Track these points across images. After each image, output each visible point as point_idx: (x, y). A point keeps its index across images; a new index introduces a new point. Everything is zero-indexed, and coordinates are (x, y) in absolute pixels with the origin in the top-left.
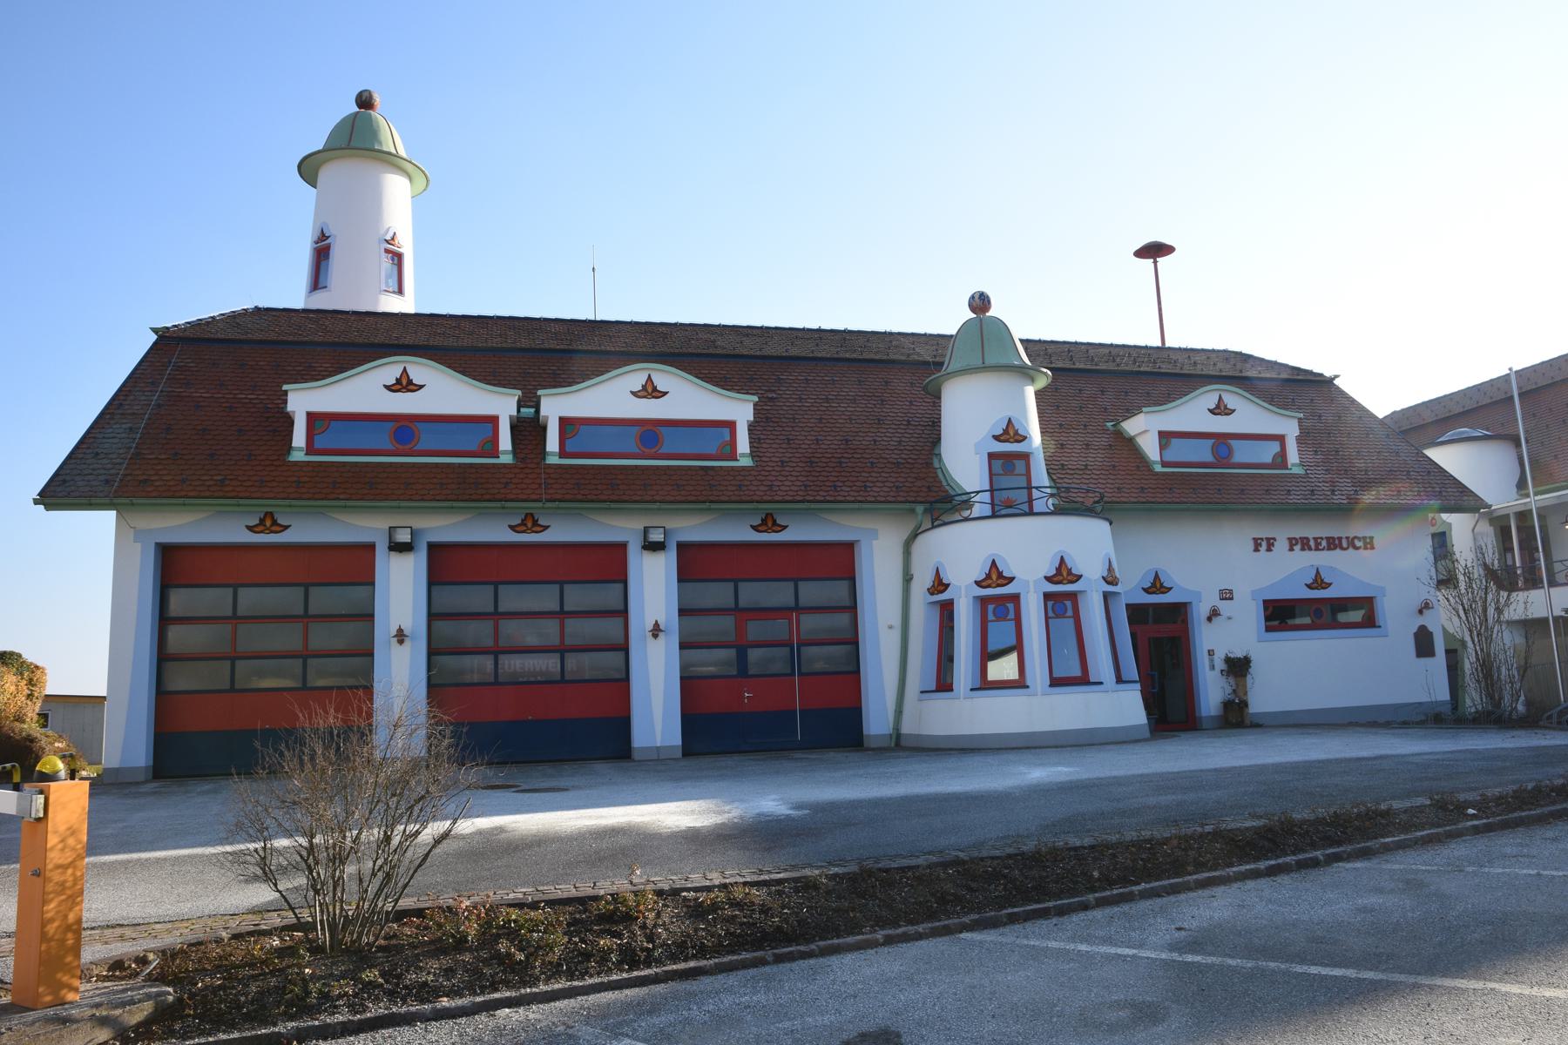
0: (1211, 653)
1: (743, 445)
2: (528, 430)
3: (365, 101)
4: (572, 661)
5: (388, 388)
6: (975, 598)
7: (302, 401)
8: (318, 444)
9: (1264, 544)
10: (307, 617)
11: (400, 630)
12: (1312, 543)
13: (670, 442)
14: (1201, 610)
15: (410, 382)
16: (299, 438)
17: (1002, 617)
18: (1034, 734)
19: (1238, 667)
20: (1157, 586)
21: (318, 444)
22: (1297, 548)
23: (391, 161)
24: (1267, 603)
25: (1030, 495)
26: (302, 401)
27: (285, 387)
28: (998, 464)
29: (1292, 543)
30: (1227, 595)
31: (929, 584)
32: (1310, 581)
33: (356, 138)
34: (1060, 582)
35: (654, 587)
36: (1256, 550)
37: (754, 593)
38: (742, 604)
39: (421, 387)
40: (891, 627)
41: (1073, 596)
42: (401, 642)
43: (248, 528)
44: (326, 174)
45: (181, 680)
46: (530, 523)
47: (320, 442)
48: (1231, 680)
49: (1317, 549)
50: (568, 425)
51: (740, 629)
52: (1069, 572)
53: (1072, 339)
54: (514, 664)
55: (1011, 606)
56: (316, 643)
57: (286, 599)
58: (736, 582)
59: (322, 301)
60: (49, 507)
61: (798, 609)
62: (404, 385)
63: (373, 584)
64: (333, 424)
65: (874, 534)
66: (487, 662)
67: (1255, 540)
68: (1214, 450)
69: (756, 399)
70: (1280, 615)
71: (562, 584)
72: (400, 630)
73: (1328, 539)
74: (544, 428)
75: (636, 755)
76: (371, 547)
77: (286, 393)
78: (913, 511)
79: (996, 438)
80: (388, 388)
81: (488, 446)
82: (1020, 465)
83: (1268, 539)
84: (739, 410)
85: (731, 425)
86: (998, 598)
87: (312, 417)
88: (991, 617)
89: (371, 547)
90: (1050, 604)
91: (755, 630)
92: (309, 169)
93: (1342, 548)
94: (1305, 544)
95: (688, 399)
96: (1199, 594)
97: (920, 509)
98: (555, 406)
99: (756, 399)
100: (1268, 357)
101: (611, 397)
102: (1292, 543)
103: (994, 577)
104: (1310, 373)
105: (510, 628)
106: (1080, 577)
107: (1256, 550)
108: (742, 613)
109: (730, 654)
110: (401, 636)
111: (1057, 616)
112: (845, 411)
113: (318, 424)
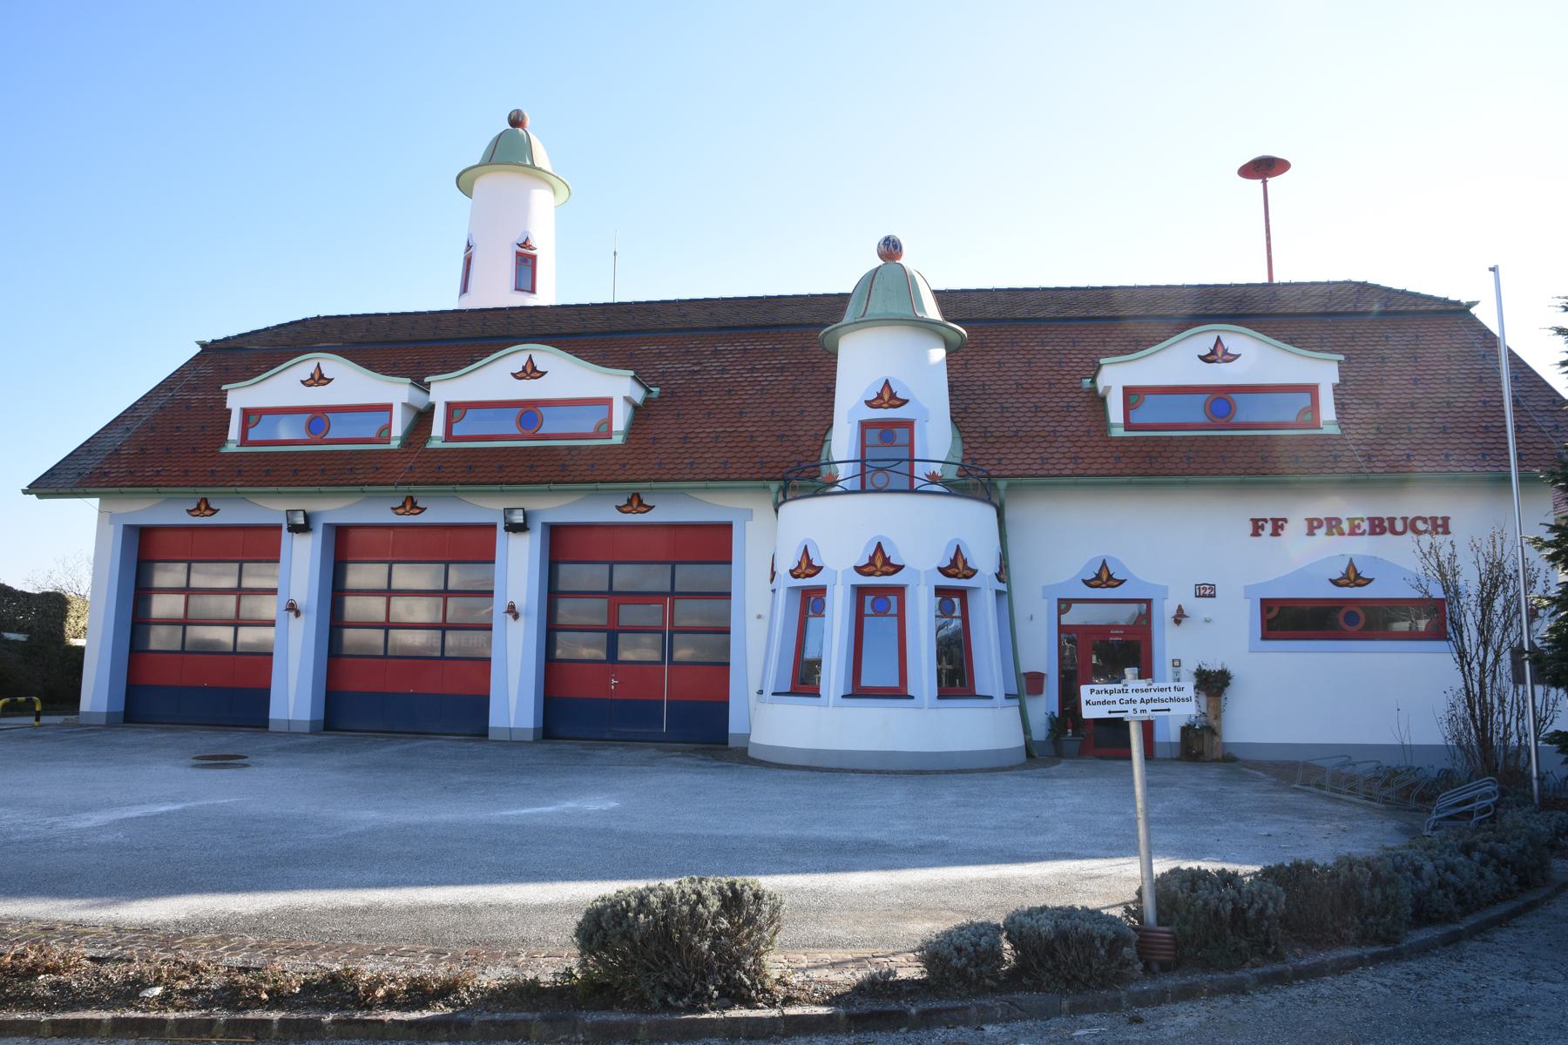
0: (1177, 664)
1: (1328, 411)
2: (422, 418)
3: (516, 121)
4: (452, 638)
5: (514, 375)
7: (1115, 377)
8: (252, 436)
9: (1269, 527)
12: (1345, 526)
13: (339, 428)
14: (1163, 612)
15: (534, 369)
16: (234, 432)
17: (881, 612)
19: (1213, 683)
20: (1104, 578)
21: (252, 436)
22: (1320, 532)
24: (1267, 605)
25: (912, 468)
26: (1115, 377)
27: (427, 380)
28: (873, 435)
29: (1312, 526)
30: (1206, 592)
32: (1088, 578)
33: (509, 149)
34: (955, 576)
35: (518, 566)
36: (1256, 534)
37: (627, 576)
38: (616, 588)
40: (759, 617)
43: (618, 508)
44: (483, 184)
45: (568, 646)
46: (636, 502)
48: (1203, 699)
49: (1352, 533)
50: (1132, 395)
51: (613, 613)
53: (1131, 283)
55: (893, 599)
57: (654, 578)
58: (611, 564)
59: (474, 301)
60: (40, 496)
61: (674, 594)
62: (530, 372)
63: (729, 562)
65: (749, 514)
66: (378, 635)
67: (1255, 521)
68: (521, 421)
69: (1342, 358)
70: (1287, 620)
71: (673, 564)
73: (1371, 520)
74: (1103, 400)
75: (731, 745)
76: (493, 527)
77: (1100, 366)
78: (766, 488)
79: (869, 403)
81: (604, 429)
82: (901, 433)
84: (1323, 372)
85: (1312, 390)
86: (878, 592)
87: (247, 413)
88: (868, 610)
89: (493, 527)
91: (630, 614)
92: (465, 182)
93: (1394, 532)
94: (1333, 525)
95: (566, 376)
96: (1165, 589)
97: (774, 486)
98: (445, 390)
99: (632, 373)
100: (1395, 287)
101: (492, 380)
102: (1312, 526)
104: (1445, 301)
105: (399, 604)
106: (820, 568)
107: (1256, 534)
108: (616, 598)
110: (512, 611)
112: (736, 380)
113: (457, 413)
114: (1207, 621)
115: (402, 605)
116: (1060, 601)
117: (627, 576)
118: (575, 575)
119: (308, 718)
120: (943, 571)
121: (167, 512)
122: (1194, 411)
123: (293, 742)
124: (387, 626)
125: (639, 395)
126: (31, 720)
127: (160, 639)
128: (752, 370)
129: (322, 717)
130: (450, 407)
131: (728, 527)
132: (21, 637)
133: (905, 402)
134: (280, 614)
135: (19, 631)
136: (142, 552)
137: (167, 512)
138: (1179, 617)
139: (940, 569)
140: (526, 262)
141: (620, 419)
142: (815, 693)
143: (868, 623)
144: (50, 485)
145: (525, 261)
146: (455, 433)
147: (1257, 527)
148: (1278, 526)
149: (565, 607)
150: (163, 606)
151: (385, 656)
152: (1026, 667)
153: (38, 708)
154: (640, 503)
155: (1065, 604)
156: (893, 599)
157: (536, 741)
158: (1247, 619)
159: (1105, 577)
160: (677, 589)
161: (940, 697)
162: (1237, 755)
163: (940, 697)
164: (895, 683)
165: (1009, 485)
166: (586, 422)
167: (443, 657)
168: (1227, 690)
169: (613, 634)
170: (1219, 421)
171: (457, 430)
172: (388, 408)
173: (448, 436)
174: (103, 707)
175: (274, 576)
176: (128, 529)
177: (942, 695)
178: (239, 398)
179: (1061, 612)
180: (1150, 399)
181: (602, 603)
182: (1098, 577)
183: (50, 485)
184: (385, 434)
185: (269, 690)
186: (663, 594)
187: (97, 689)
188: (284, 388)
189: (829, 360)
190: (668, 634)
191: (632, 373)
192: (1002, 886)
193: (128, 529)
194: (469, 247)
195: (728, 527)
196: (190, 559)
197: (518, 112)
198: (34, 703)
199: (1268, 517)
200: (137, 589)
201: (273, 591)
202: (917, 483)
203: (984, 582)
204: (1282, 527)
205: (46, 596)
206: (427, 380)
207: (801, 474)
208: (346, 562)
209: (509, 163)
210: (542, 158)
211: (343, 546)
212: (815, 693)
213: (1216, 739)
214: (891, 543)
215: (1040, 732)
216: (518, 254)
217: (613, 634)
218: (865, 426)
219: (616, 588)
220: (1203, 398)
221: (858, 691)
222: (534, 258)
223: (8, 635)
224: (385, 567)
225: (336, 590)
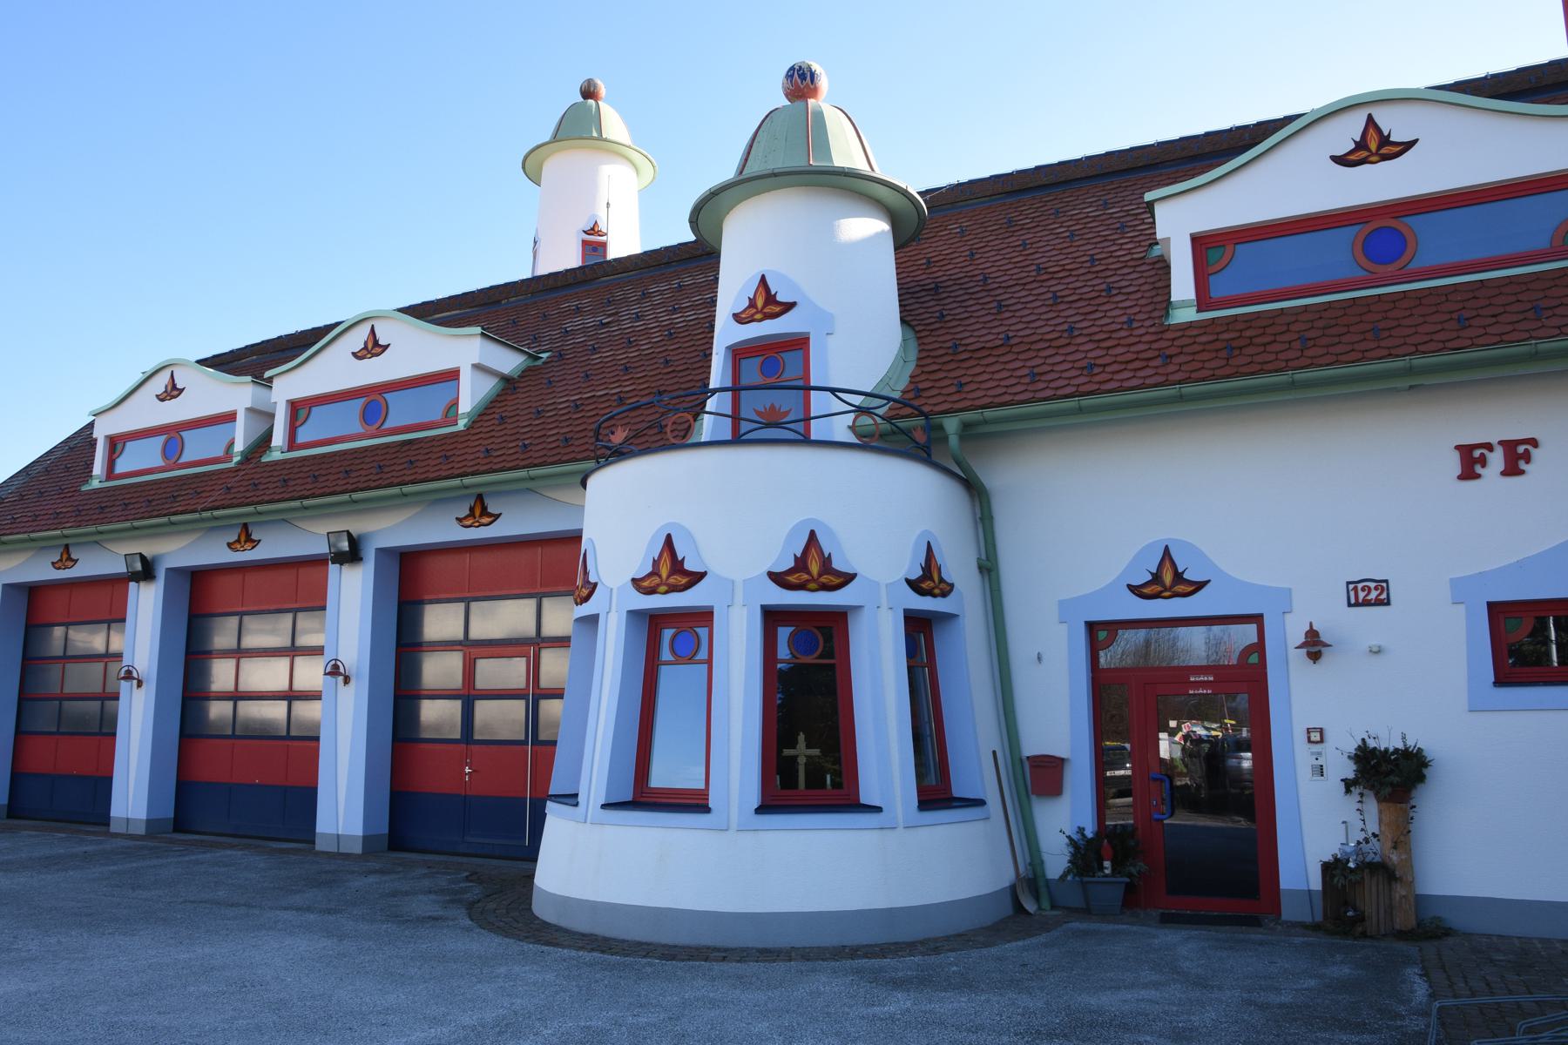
3: (589, 92)
5: (1341, 160)
9: (1497, 460)
13: (1435, 243)
14: (1287, 634)
16: (1182, 285)
19: (1391, 775)
20: (1167, 578)
21: (301, 439)
23: (612, 149)
27: (1148, 197)
28: (752, 371)
30: (1370, 594)
33: (578, 126)
39: (1409, 145)
42: (1315, 657)
44: (552, 167)
46: (480, 511)
47: (1219, 288)
52: (826, 562)
54: (251, 710)
77: (1150, 206)
80: (1341, 160)
83: (1509, 446)
87: (1203, 244)
88: (666, 655)
90: (784, 633)
91: (491, 672)
103: (815, 568)
108: (472, 649)
109: (517, 708)
113: (1213, 255)
114: (1377, 651)
116: (1092, 627)
119: (357, 829)
120: (915, 585)
122: (1337, 255)
124: (291, 696)
125: (509, 361)
127: (437, 714)
138: (1314, 646)
139: (908, 581)
141: (471, 395)
143: (667, 675)
145: (595, 250)
147: (1471, 462)
148: (1517, 457)
150: (440, 670)
152: (1033, 745)
155: (1099, 633)
158: (1462, 645)
159: (1168, 578)
161: (761, 810)
162: (1455, 920)
163: (761, 810)
164: (702, 786)
165: (966, 426)
168: (1420, 786)
170: (1380, 269)
171: (1219, 288)
175: (321, 630)
179: (1094, 648)
180: (131, 446)
182: (1157, 578)
184: (451, 414)
185: (316, 789)
186: (459, 643)
196: (469, 594)
197: (590, 82)
199: (1494, 439)
202: (745, 427)
203: (967, 599)
204: (1527, 457)
206: (267, 374)
208: (422, 602)
211: (410, 581)
213: (1400, 891)
214: (689, 535)
215: (1056, 860)
216: (584, 243)
220: (1348, 233)
221: (642, 796)
224: (532, 603)
225: (403, 644)
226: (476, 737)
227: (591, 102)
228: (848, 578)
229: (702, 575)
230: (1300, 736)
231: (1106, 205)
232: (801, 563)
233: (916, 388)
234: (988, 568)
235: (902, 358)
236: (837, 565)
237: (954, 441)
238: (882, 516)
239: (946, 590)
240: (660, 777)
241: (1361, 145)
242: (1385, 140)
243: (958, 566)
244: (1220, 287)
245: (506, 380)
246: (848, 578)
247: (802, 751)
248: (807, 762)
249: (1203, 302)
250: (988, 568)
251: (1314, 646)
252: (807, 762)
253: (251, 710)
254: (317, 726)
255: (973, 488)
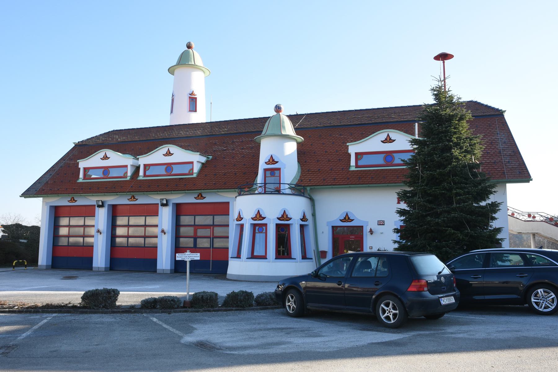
3: (189, 46)
4: (131, 240)
5: (382, 142)
6: (251, 224)
7: (354, 148)
10: (145, 226)
11: (371, 230)
14: (366, 230)
17: (260, 232)
18: (239, 275)
20: (347, 218)
23: (195, 67)
26: (354, 148)
27: (348, 144)
28: (268, 173)
30: (381, 223)
31: (236, 217)
33: (184, 60)
34: (283, 220)
37: (200, 220)
41: (288, 225)
42: (372, 234)
44: (177, 72)
46: (200, 196)
50: (359, 155)
51: (195, 232)
52: (287, 216)
56: (131, 233)
58: (214, 216)
60: (25, 197)
61: (214, 225)
64: (364, 156)
72: (371, 230)
75: (158, 272)
80: (382, 142)
81: (191, 172)
82: (277, 172)
86: (259, 226)
87: (357, 154)
88: (257, 231)
91: (201, 232)
92: (171, 70)
95: (180, 155)
98: (143, 160)
101: (157, 157)
103: (285, 217)
108: (196, 227)
111: (259, 232)
115: (129, 230)
116: (333, 227)
117: (200, 220)
118: (186, 220)
119: (169, 268)
120: (301, 220)
121: (62, 201)
123: (99, 273)
125: (203, 159)
126: (24, 268)
128: (242, 149)
129: (51, 264)
130: (145, 166)
131: (229, 203)
132: (25, 241)
133: (277, 162)
134: (96, 232)
135: (24, 239)
136: (56, 214)
137: (62, 201)
139: (278, 218)
140: (193, 100)
141: (196, 168)
142: (240, 258)
143: (257, 235)
144: (28, 194)
145: (193, 100)
146: (147, 174)
149: (182, 230)
151: (128, 246)
152: (321, 249)
153: (26, 264)
154: (202, 196)
156: (264, 228)
157: (171, 273)
159: (347, 218)
160: (215, 224)
161: (276, 259)
163: (276, 259)
164: (264, 254)
165: (311, 189)
166: (185, 169)
167: (145, 247)
169: (195, 238)
172: (126, 166)
173: (145, 175)
174: (45, 264)
176: (51, 207)
177: (277, 258)
178: (83, 164)
181: (192, 228)
182: (345, 218)
183: (28, 194)
187: (43, 257)
188: (94, 161)
189: (257, 148)
190: (212, 238)
191: (199, 153)
192: (148, 295)
193: (51, 207)
194: (173, 96)
195: (229, 203)
197: (189, 43)
198: (24, 262)
200: (54, 226)
201: (93, 226)
203: (310, 222)
205: (33, 227)
207: (245, 186)
208: (180, 215)
209: (185, 64)
210: (199, 61)
212: (240, 258)
216: (190, 97)
217: (195, 238)
218: (266, 170)
219: (196, 224)
220: (383, 155)
221: (253, 257)
222: (196, 98)
223: (21, 240)
225: (113, 226)
226: (198, 246)
227: (190, 50)
228: (291, 219)
229: (265, 218)
230: (368, 248)
231: (341, 135)
232: (283, 216)
233: (301, 180)
234: (314, 215)
235: (298, 172)
236: (289, 216)
237: (309, 192)
238: (296, 206)
239: (307, 220)
240: (255, 254)
241: (386, 139)
242: (390, 139)
243: (309, 216)
244: (360, 163)
245: (203, 164)
246: (291, 219)
247: (281, 249)
248: (283, 251)
249: (357, 166)
250: (314, 215)
251: (371, 232)
252: (283, 251)
253: (72, 240)
254: (157, 244)
255: (312, 200)
